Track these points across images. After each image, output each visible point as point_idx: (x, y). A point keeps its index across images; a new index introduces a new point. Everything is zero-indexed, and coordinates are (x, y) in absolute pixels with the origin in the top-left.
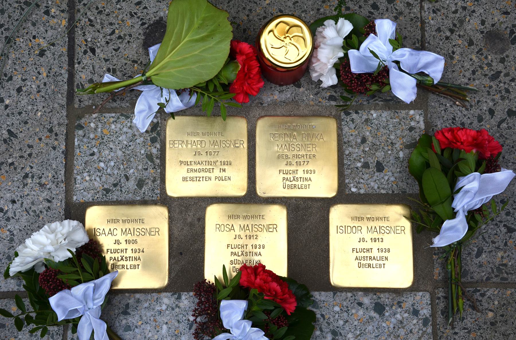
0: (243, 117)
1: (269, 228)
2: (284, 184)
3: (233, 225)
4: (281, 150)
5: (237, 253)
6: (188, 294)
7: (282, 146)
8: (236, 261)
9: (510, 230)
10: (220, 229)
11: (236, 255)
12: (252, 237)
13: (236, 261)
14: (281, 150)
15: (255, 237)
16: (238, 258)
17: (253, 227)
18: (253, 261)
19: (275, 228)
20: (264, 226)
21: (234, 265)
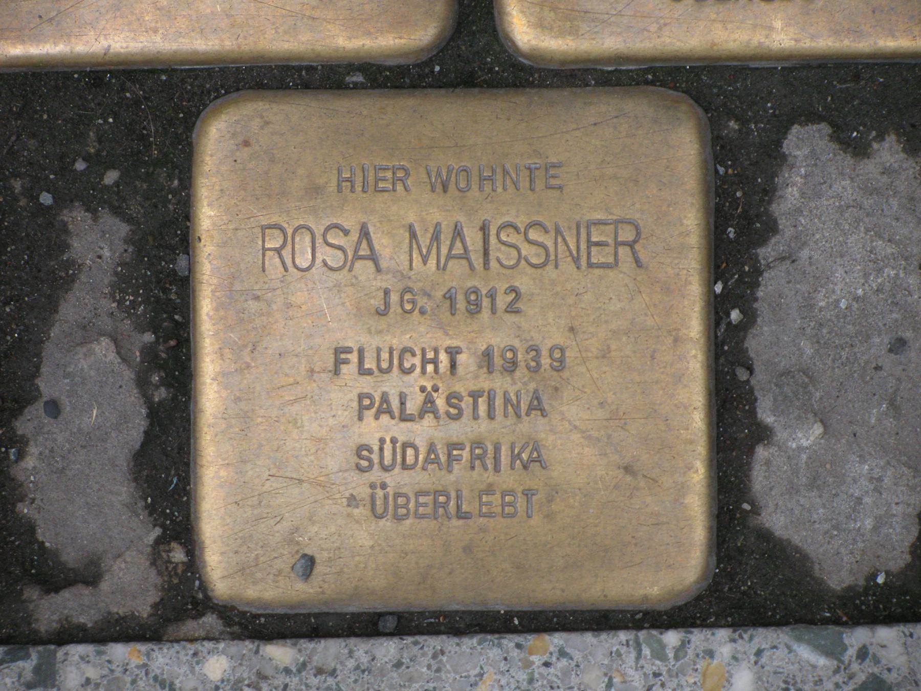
0: (202, 582)
1: (590, 244)
2: (380, 493)
3: (365, 233)
4: (432, 262)
5: (395, 403)
6: (100, 653)
7: (436, 237)
8: (388, 447)
9: (919, 663)
10: (286, 254)
11: (389, 412)
12: (486, 302)
13: (388, 447)
14: (432, 262)
15: (502, 301)
16: (400, 431)
17: (493, 240)
18: (497, 449)
19: (631, 245)
20: (558, 231)
21: (376, 475)
